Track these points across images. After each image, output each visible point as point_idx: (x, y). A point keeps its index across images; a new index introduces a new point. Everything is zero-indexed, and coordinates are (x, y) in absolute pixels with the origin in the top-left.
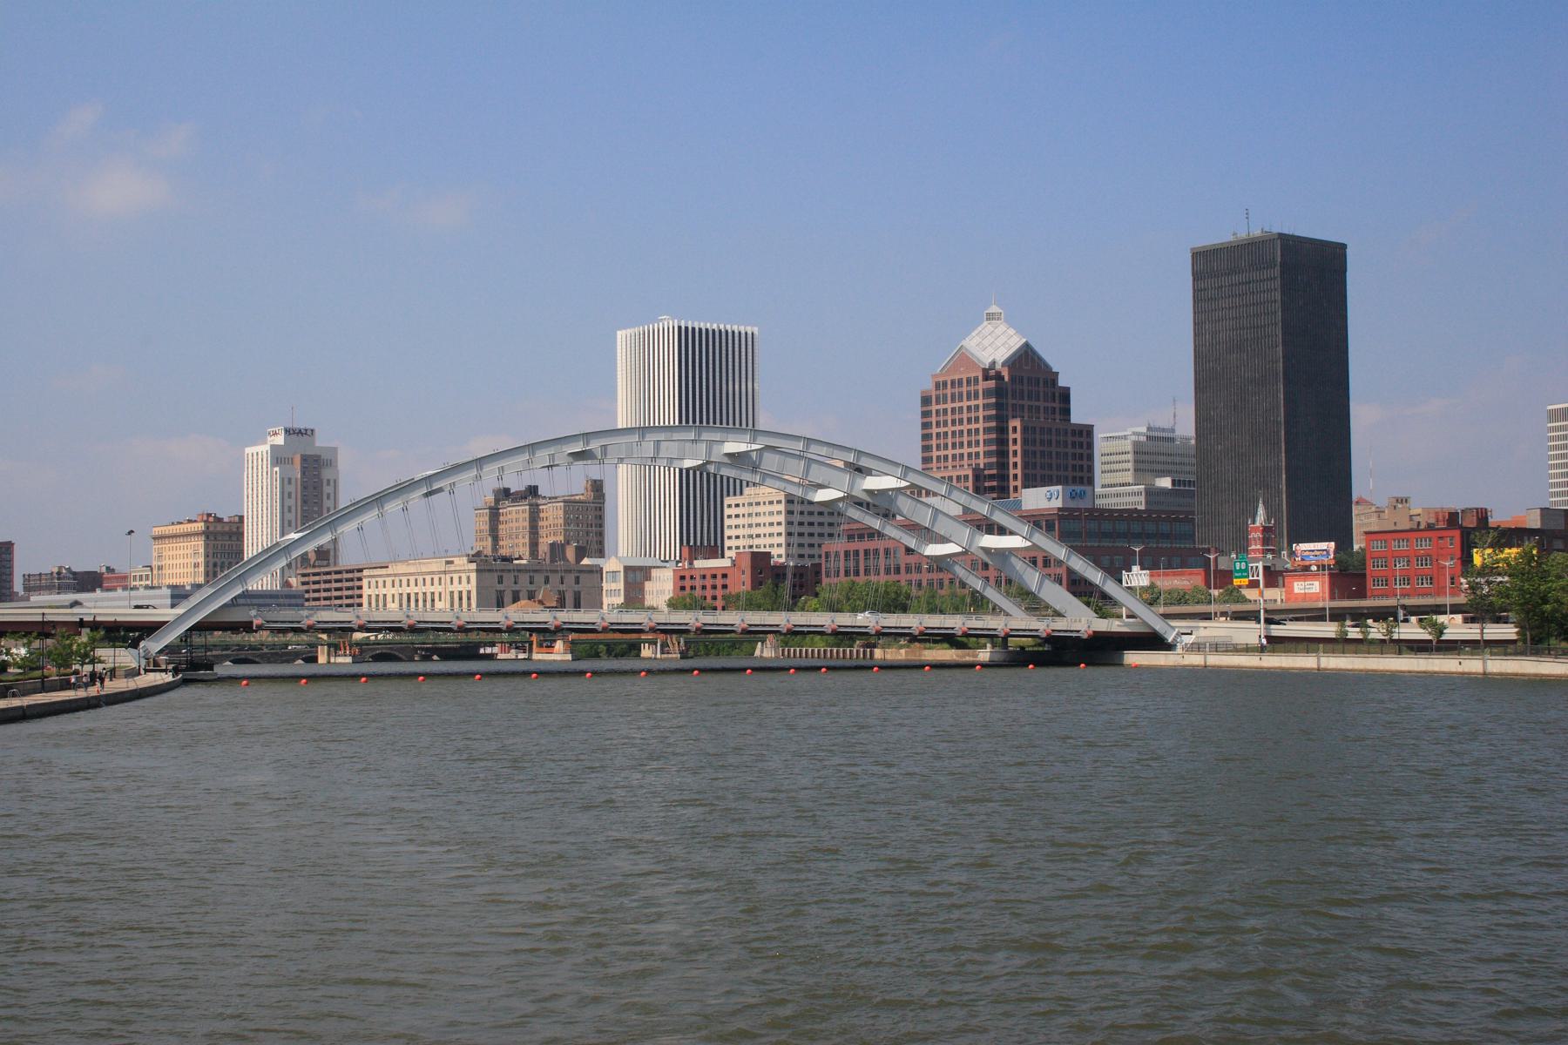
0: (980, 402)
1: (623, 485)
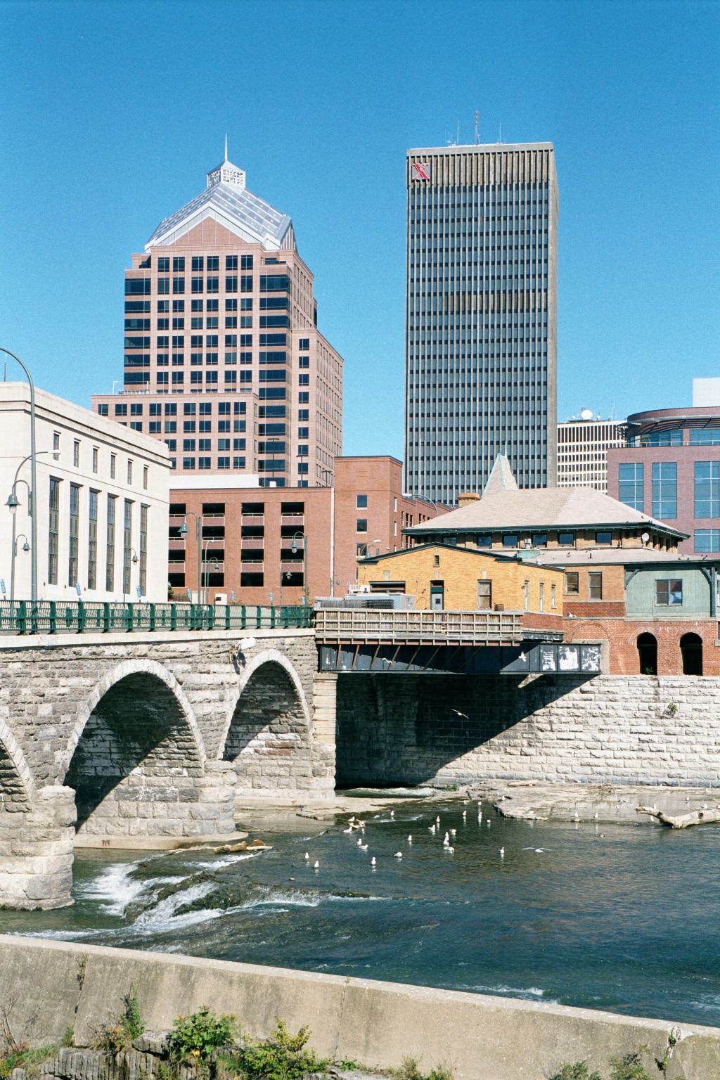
0: (256, 295)
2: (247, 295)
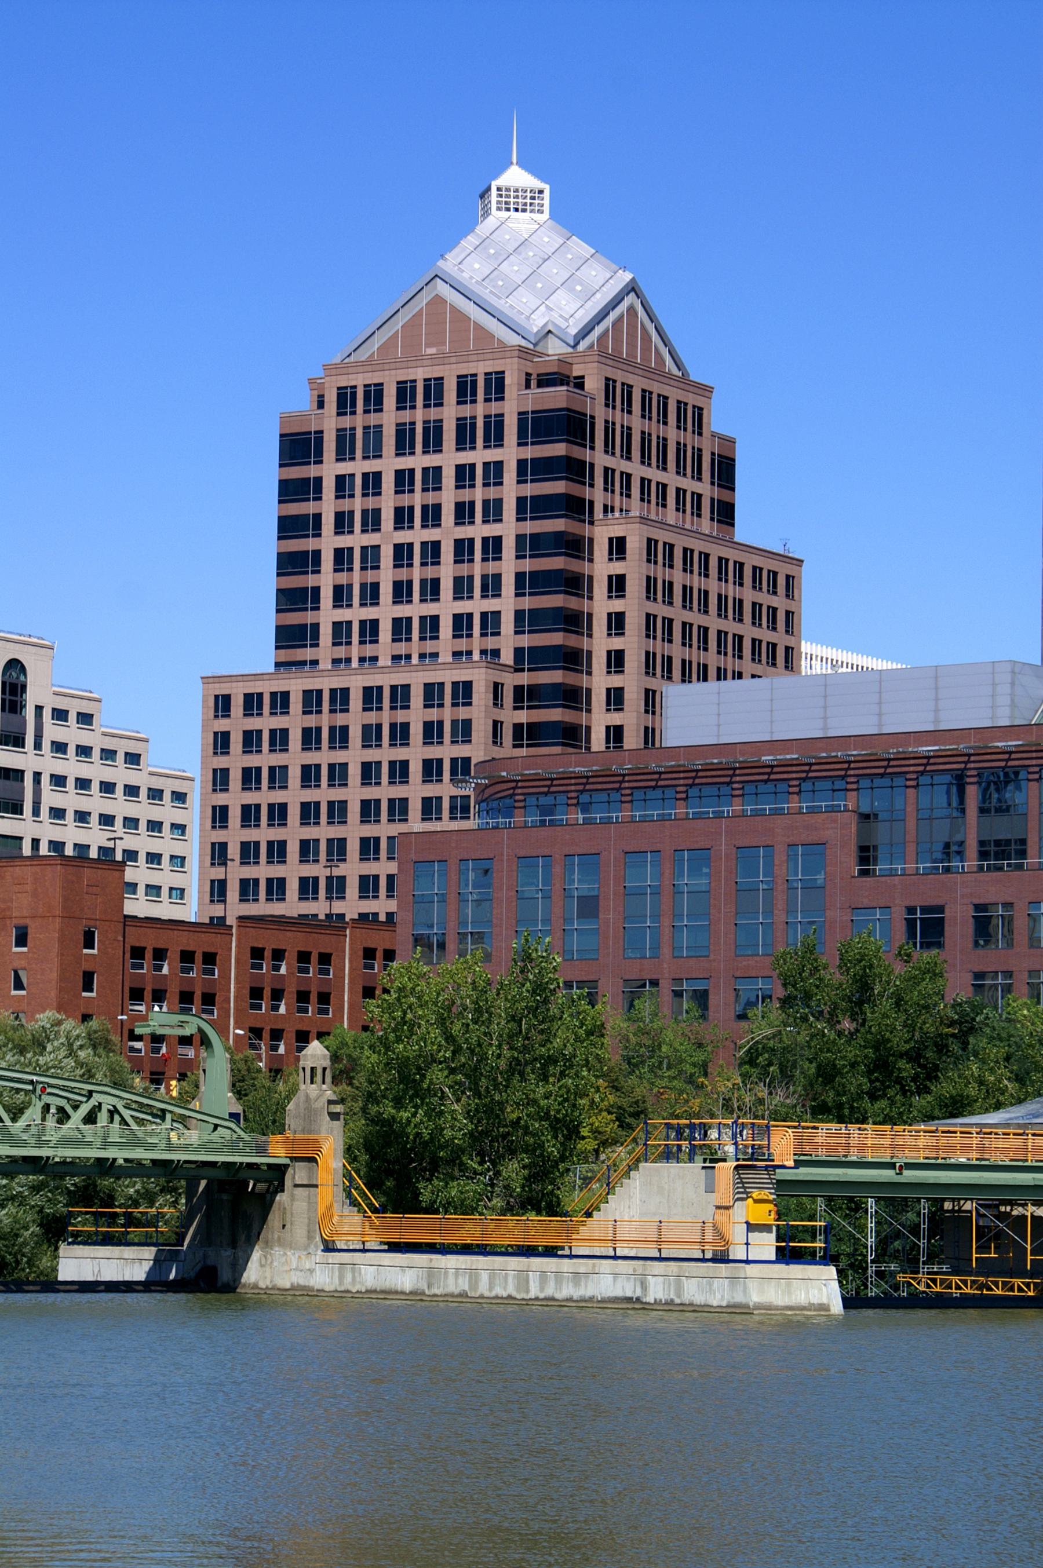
0: (510, 453)
1: (601, 516)
2: (493, 455)
